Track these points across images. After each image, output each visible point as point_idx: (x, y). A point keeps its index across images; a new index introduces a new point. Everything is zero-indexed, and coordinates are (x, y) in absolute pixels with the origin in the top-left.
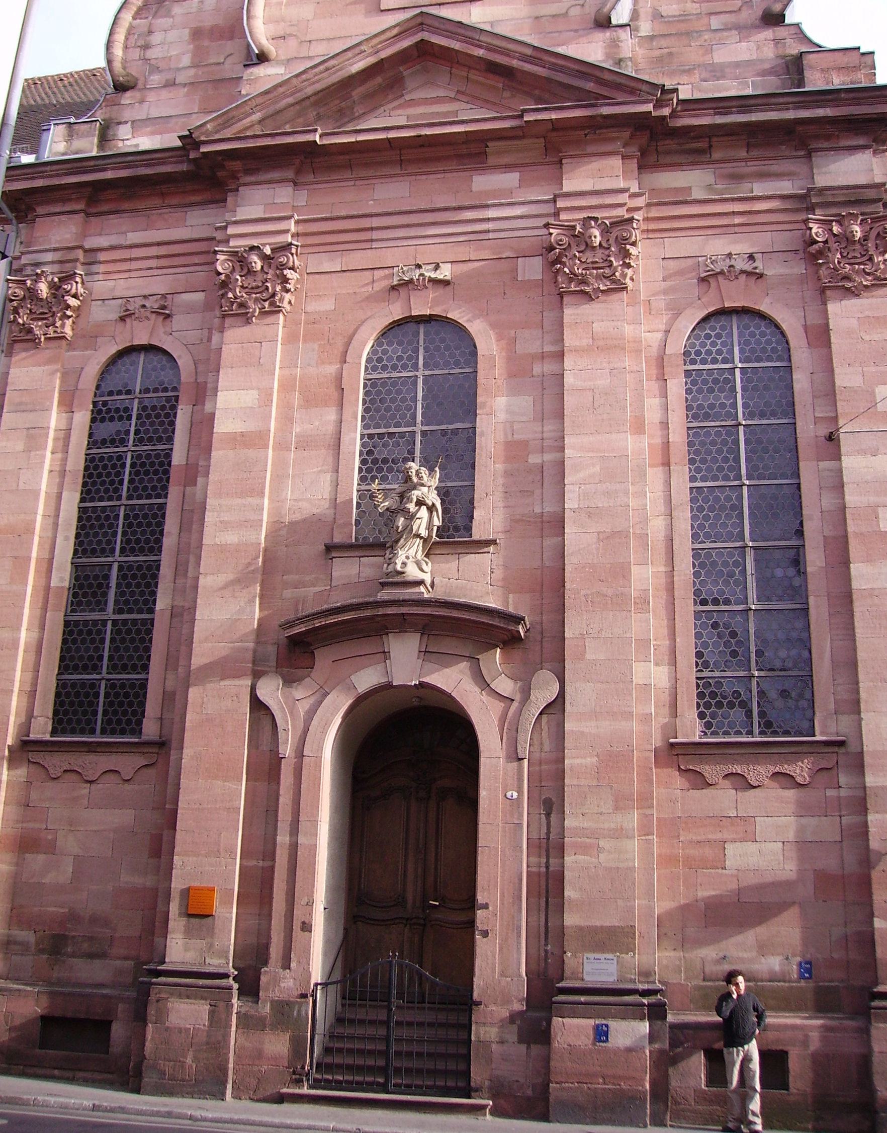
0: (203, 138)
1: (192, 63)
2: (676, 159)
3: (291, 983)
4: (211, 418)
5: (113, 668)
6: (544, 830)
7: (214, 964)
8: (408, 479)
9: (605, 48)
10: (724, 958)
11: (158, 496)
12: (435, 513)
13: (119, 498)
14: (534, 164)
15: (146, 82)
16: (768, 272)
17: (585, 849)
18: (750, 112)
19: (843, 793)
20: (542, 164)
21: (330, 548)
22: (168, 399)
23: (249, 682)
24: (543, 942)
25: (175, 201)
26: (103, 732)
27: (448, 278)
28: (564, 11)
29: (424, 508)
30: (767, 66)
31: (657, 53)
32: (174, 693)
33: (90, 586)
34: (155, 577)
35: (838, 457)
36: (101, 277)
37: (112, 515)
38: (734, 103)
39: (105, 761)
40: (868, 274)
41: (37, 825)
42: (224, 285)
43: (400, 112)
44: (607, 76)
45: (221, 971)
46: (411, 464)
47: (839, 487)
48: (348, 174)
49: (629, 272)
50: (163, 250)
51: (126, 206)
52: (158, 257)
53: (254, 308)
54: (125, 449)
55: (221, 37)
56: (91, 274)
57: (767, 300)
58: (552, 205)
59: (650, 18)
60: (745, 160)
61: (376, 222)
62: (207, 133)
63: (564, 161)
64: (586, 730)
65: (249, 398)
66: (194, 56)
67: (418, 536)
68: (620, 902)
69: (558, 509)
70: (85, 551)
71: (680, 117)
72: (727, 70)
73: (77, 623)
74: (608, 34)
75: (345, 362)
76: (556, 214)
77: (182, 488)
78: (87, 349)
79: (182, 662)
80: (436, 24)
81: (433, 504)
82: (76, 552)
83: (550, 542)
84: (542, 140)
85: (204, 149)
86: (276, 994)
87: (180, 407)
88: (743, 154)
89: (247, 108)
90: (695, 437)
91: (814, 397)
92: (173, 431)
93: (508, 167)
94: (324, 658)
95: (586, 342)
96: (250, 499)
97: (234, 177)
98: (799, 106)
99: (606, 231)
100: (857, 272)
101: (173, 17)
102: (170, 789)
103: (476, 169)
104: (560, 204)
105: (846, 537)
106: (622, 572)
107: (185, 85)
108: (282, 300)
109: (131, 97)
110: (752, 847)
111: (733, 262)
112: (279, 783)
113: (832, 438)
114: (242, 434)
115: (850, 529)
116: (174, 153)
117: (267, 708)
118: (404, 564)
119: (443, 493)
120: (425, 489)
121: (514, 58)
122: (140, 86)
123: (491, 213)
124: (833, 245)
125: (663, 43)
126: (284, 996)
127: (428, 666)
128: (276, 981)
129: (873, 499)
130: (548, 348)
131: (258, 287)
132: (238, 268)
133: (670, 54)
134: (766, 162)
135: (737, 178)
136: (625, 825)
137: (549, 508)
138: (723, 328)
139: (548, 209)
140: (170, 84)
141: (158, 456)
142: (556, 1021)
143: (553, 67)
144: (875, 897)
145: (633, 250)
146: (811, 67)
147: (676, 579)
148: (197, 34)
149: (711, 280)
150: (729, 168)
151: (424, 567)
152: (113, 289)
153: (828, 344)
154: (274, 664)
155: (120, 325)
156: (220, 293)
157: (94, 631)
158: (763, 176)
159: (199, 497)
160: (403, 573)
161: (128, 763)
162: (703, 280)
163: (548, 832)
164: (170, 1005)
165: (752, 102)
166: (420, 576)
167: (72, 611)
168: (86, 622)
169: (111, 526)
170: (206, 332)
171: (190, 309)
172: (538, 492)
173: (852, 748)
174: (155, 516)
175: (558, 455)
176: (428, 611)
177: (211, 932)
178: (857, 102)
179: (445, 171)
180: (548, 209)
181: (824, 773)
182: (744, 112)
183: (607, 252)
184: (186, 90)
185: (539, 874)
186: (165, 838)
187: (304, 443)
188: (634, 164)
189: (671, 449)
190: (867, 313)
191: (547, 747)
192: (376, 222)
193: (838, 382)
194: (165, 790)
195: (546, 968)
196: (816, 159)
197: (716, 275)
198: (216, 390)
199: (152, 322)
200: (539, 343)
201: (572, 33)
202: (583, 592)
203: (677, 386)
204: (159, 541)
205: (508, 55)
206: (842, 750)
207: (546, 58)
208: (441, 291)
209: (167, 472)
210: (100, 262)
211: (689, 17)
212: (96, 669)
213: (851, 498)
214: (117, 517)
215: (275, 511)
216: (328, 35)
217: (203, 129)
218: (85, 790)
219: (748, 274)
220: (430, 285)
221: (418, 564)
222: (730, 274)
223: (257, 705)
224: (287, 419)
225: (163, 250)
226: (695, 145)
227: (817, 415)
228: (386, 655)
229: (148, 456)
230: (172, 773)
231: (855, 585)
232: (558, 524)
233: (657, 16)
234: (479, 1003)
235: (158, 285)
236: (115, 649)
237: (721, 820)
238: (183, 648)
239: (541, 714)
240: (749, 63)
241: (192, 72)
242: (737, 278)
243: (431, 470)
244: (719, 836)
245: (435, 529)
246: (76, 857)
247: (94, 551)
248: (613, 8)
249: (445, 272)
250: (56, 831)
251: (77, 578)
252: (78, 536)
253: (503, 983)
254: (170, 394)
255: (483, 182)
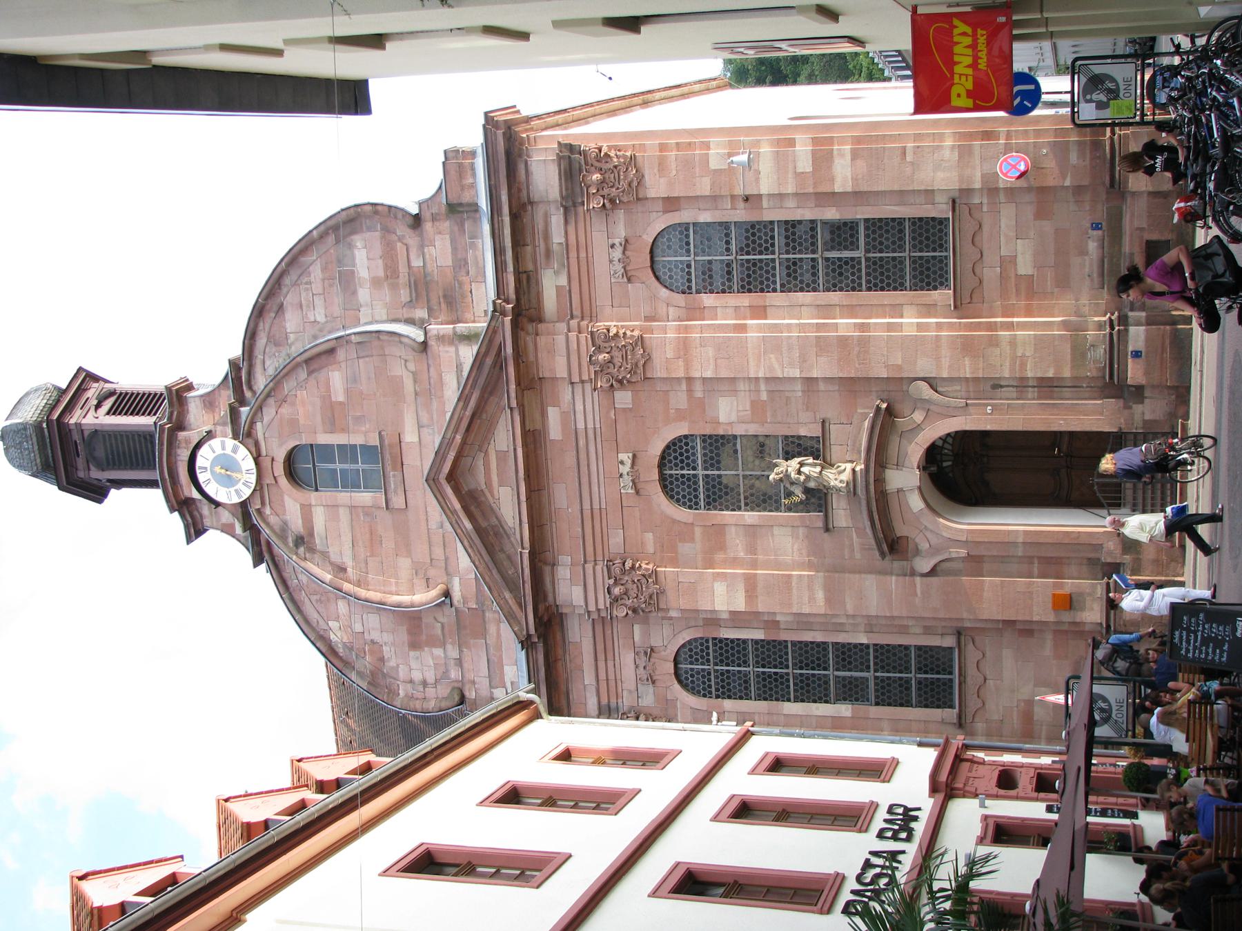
0: (525, 633)
1: (441, 647)
2: (533, 294)
3: (1111, 543)
4: (732, 613)
5: (908, 670)
6: (1011, 389)
7: (1100, 591)
8: (781, 480)
9: (444, 345)
10: (1089, 276)
11: (786, 647)
12: (806, 462)
13: (787, 674)
14: (541, 397)
15: (457, 681)
16: (623, 234)
17: (1023, 365)
18: (504, 247)
19: (985, 201)
20: (541, 391)
21: (827, 530)
22: (714, 645)
23: (918, 579)
24: (1082, 389)
25: (560, 652)
26: (951, 673)
27: (630, 455)
28: (411, 375)
29: (802, 469)
30: (456, 228)
31: (443, 306)
32: (925, 627)
33: (850, 689)
34: (843, 645)
35: (760, 196)
36: (620, 701)
37: (800, 678)
38: (499, 259)
39: (971, 671)
40: (627, 169)
41: (1015, 713)
42: (635, 611)
43: (496, 493)
44: (483, 350)
45: (1105, 587)
46: (771, 478)
47: (781, 196)
48: (547, 528)
49: (629, 333)
50: (601, 657)
51: (563, 688)
52: (606, 660)
53: (654, 588)
54: (752, 673)
55: (419, 627)
56: (618, 708)
57: (645, 237)
58: (575, 385)
59: (413, 310)
60: (535, 247)
61: (587, 506)
62: (521, 630)
63: (541, 376)
64: (948, 364)
65: (720, 588)
66: (435, 646)
67: (821, 472)
68: (1056, 343)
69: (800, 381)
70: (826, 695)
71: (508, 296)
72: (459, 256)
73: (877, 697)
74: (432, 343)
75: (692, 524)
76: (582, 382)
77: (781, 631)
78: (676, 706)
79: (905, 622)
80: (435, 470)
81: (799, 463)
82: (826, 702)
83: (822, 386)
84: (525, 392)
85: (532, 631)
86: (1118, 551)
87: (722, 636)
88: (529, 249)
89: (502, 602)
90: (746, 288)
91: (716, 209)
92: (738, 640)
93: (544, 414)
94: (901, 530)
95: (681, 363)
96: (793, 584)
97: (548, 608)
98: (500, 213)
99: (599, 349)
100: (626, 177)
101: (398, 665)
102: (989, 625)
103: (545, 438)
104: (576, 379)
105: (816, 194)
106: (843, 341)
107: (461, 651)
108: (647, 570)
109: (469, 690)
110: (1020, 259)
111: (616, 259)
112: (984, 556)
113: (747, 199)
114: (747, 591)
115: (811, 190)
116: (530, 654)
117: (935, 566)
118: (841, 481)
119: (788, 456)
120: (790, 469)
121: (464, 414)
122: (460, 685)
123: (581, 425)
124: (606, 192)
125: (434, 301)
126: (1120, 547)
127: (907, 463)
128: (1110, 553)
129: (790, 175)
130: (684, 387)
131: (638, 587)
132: (623, 601)
133: (445, 296)
134: (536, 232)
135: (548, 253)
136: (1008, 340)
137: (799, 387)
138: (664, 267)
139: (578, 388)
140: (459, 662)
141: (757, 649)
142: (1129, 382)
143: (473, 387)
144: (1051, 185)
145: (613, 331)
146: (459, 197)
147: (845, 304)
148: (415, 645)
149: (629, 274)
150: (541, 258)
151: (842, 468)
152: (630, 692)
153: (678, 198)
154: (905, 563)
155: (657, 684)
156: (641, 613)
157: (882, 685)
158: (547, 236)
159: (790, 618)
160: (847, 483)
161: (972, 655)
162: (629, 280)
163: (1013, 386)
164: (1128, 618)
165: (498, 246)
166: (849, 470)
167: (868, 700)
168: (876, 691)
169: (808, 679)
170: (664, 622)
171: (646, 634)
172: (787, 394)
173: (956, 194)
174: (801, 649)
175: (761, 381)
176: (872, 465)
177: (1081, 594)
178: (496, 171)
179: (546, 459)
180: (578, 388)
181: (972, 212)
182: (505, 251)
183: (614, 349)
184: (465, 650)
185: (1039, 392)
186: (1021, 627)
187: (752, 549)
188: (541, 327)
189: (755, 304)
190: (656, 171)
191: (958, 388)
192: (587, 506)
193: (707, 193)
194: (989, 629)
195: (1098, 387)
196: (536, 196)
197: (626, 271)
198: (714, 611)
199: (657, 660)
200: (679, 394)
201: (432, 369)
202: (857, 366)
203: (708, 300)
204: (818, 644)
205: (462, 419)
206: (957, 201)
207: (466, 391)
208: (639, 461)
209: (768, 642)
210: (609, 702)
211: (412, 282)
212: (908, 681)
213: (790, 189)
214: (801, 675)
215: (801, 566)
216: (426, 547)
217: (518, 633)
218: (990, 683)
219: (625, 250)
220: (636, 468)
221: (840, 473)
222: (625, 261)
223: (933, 572)
224: (735, 562)
225: (601, 657)
226: (525, 282)
227: (729, 207)
228: (899, 491)
229: (757, 656)
230: (978, 625)
231: (849, 189)
232: (810, 381)
233: (411, 304)
234: (1120, 428)
235: (627, 659)
236: (894, 669)
237: (1003, 277)
238: (896, 622)
239: (936, 391)
240: (453, 241)
241: (449, 647)
242: (628, 258)
243: (776, 465)
244: (1013, 280)
245: (815, 461)
246: (1035, 686)
247: (826, 689)
248: (414, 340)
249: (626, 457)
250: (1018, 700)
251: (845, 699)
252: (815, 701)
253: (1107, 413)
254: (710, 644)
255: (555, 430)
